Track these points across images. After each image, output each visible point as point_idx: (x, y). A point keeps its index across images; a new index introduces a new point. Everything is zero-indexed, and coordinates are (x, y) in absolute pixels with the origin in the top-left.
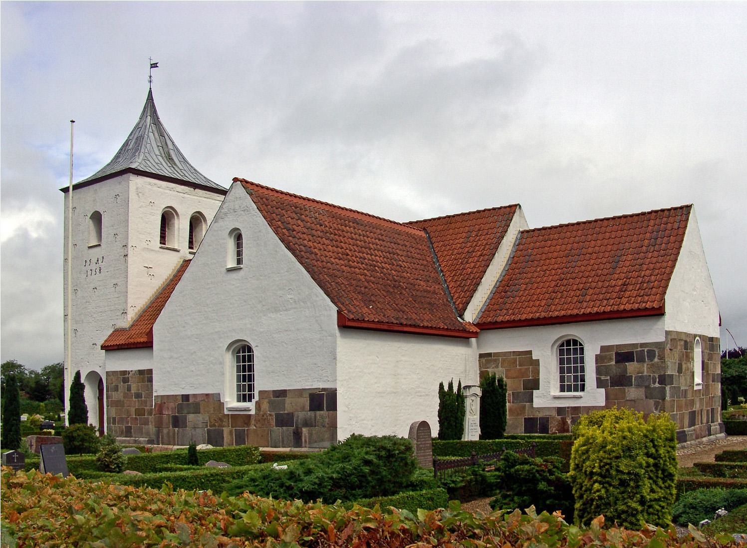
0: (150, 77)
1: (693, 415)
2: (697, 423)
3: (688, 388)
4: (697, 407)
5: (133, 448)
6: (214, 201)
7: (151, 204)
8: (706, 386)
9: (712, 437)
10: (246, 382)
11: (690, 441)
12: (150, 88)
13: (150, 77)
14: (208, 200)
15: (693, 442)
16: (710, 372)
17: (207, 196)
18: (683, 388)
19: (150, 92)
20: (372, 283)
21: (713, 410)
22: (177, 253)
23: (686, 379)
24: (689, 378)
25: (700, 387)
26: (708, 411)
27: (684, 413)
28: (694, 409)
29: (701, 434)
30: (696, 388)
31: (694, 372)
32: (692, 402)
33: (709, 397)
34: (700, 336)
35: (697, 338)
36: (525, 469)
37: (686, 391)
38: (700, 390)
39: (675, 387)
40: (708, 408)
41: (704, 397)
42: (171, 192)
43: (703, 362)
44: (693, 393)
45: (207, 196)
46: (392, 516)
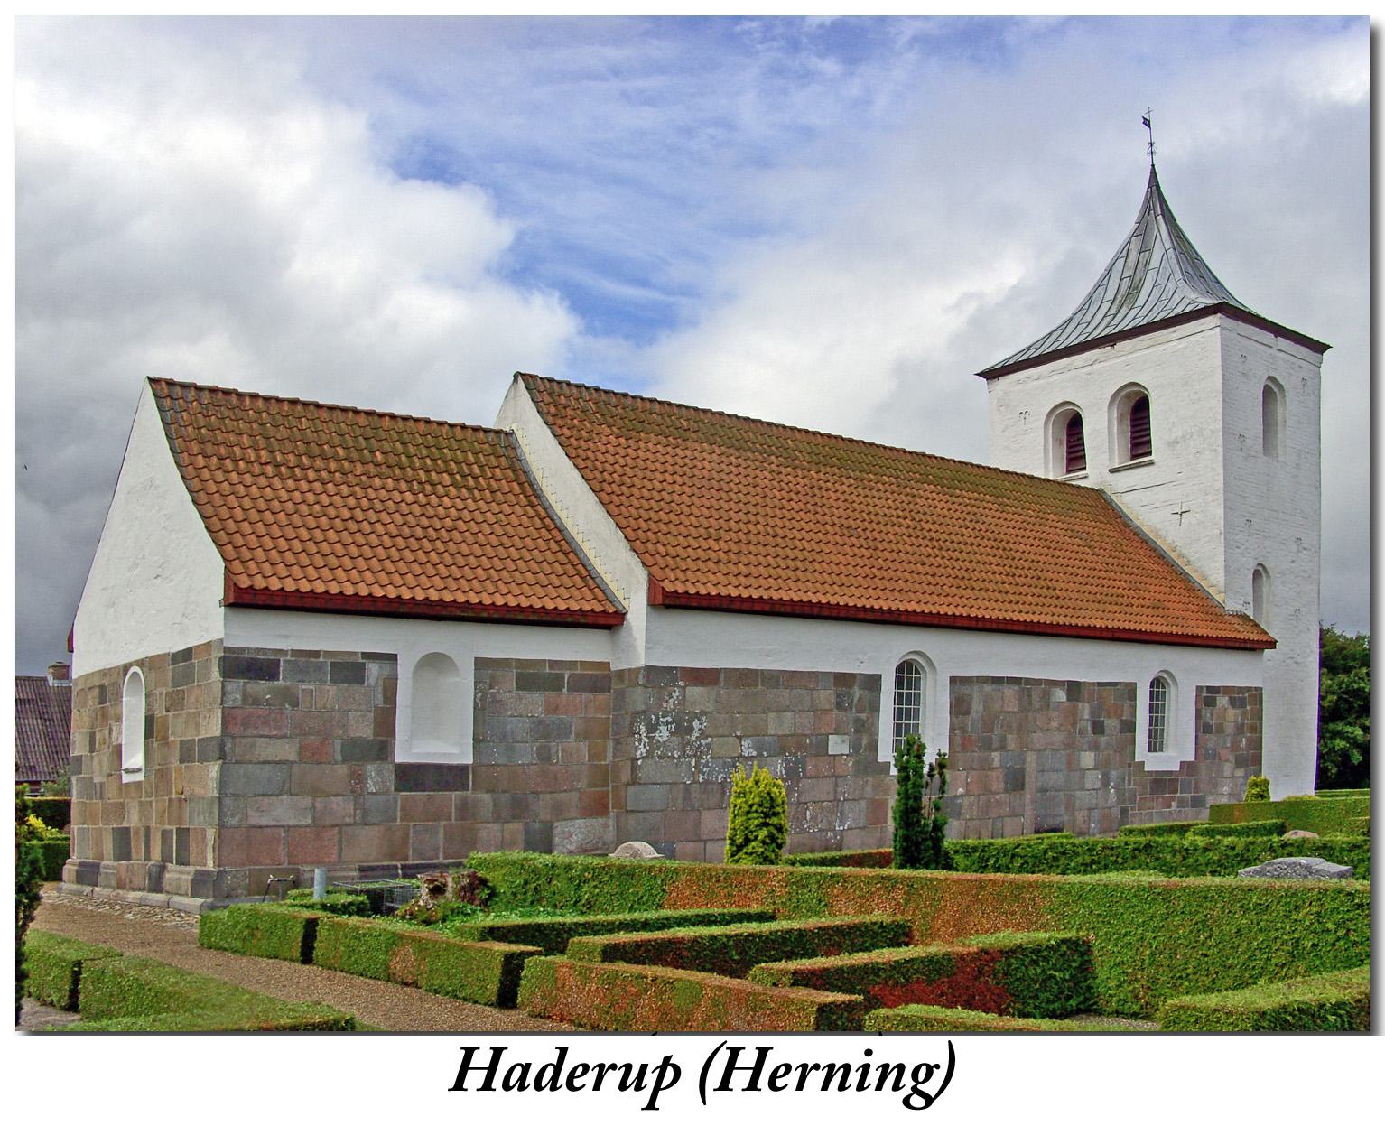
0: (1151, 144)
1: (123, 837)
2: (134, 855)
3: (104, 780)
4: (133, 820)
5: (1205, 826)
6: (1163, 347)
7: (1023, 416)
8: (159, 773)
9: (159, 897)
10: (905, 724)
11: (104, 887)
12: (1153, 166)
13: (1151, 144)
14: (1155, 349)
15: (107, 891)
16: (172, 738)
17: (1150, 342)
18: (97, 780)
19: (1153, 172)
20: (983, 486)
21: (183, 833)
22: (1151, 468)
23: (100, 763)
24: (105, 759)
25: (140, 777)
26: (165, 835)
27: (100, 828)
28: (125, 825)
29: (131, 882)
30: (126, 778)
31: (121, 745)
32: (121, 810)
33: (170, 800)
34: (141, 663)
35: (135, 669)
36: (783, 961)
37: (102, 784)
38: (140, 783)
39: (84, 778)
40: (167, 827)
41: (153, 798)
42: (1063, 376)
43: (150, 721)
44: (121, 789)
45: (1140, 345)
46: (73, 882)
